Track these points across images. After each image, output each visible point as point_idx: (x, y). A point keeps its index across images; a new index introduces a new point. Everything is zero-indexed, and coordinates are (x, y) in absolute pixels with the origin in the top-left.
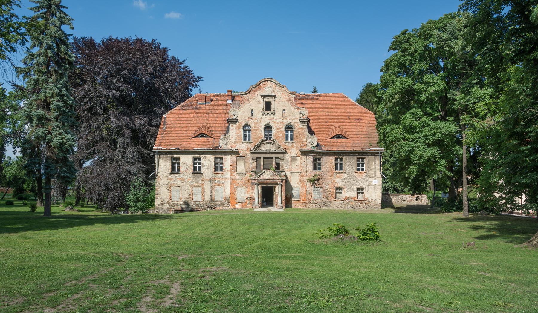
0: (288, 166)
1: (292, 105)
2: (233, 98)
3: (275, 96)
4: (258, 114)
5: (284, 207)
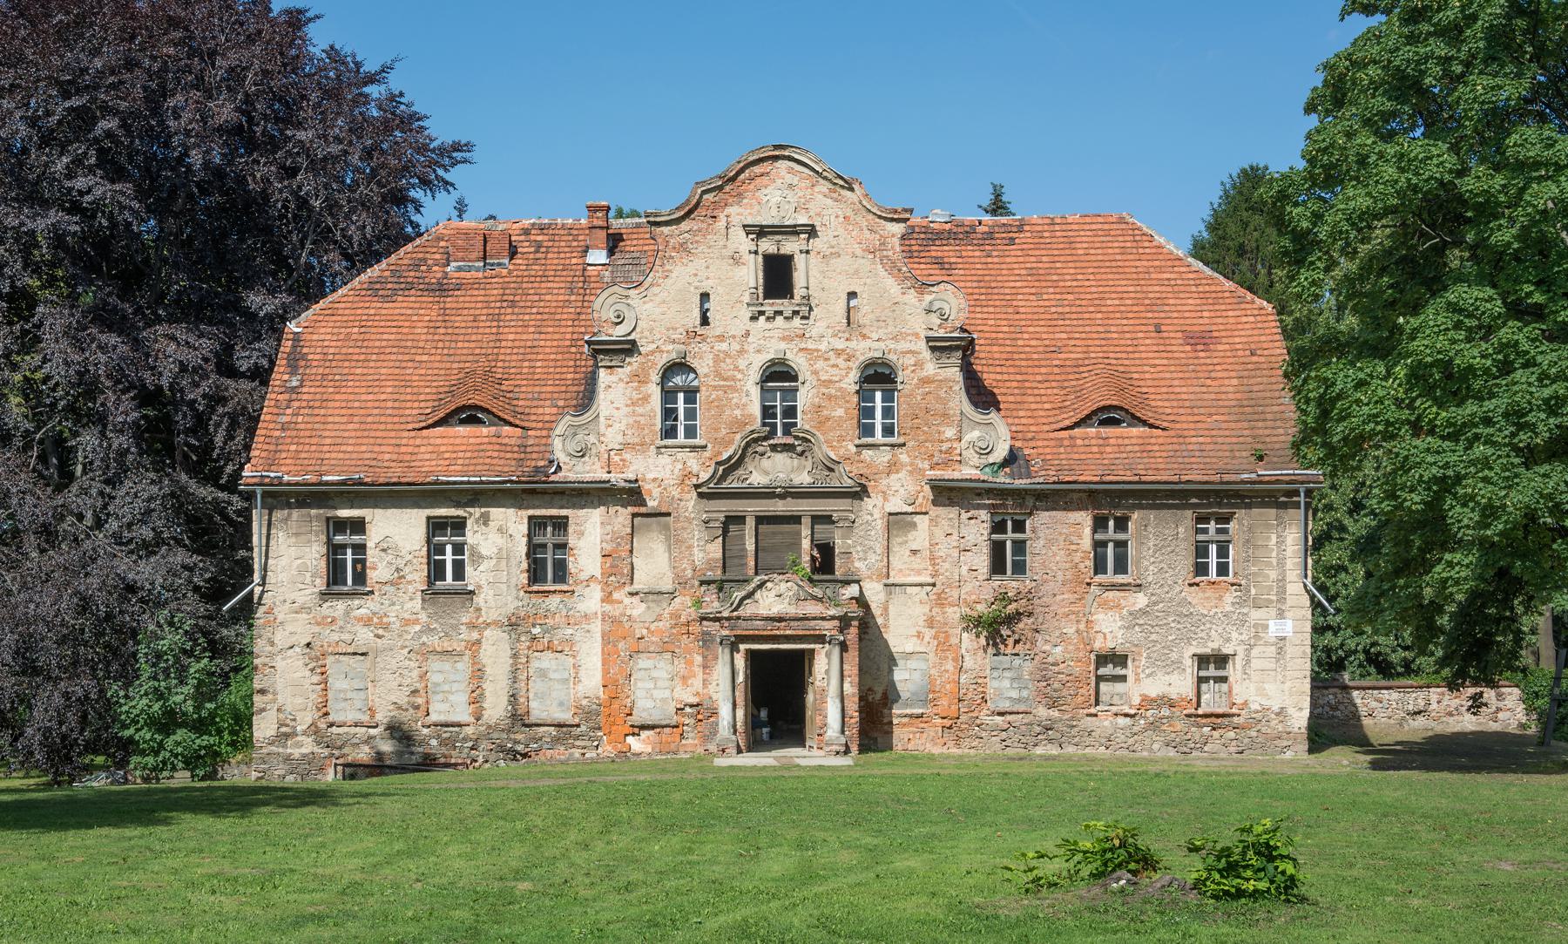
0: (872, 558)
5: (854, 748)
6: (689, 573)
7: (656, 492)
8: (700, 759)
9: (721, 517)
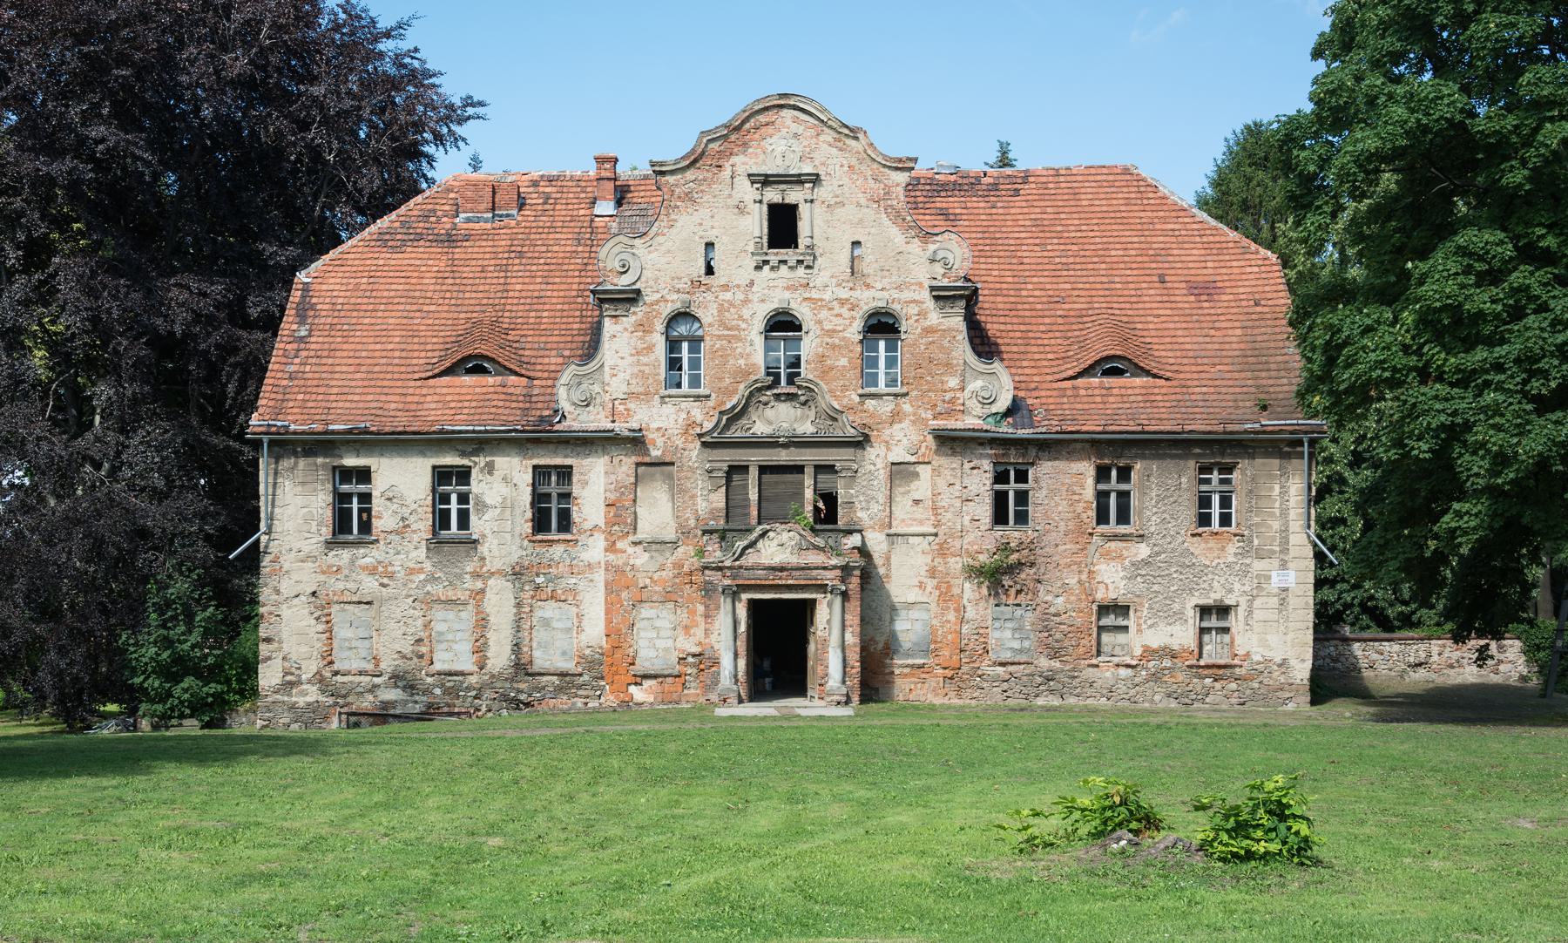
0: (875, 508)
5: (856, 698)
6: (692, 523)
7: (660, 442)
8: (701, 709)
9: (725, 466)
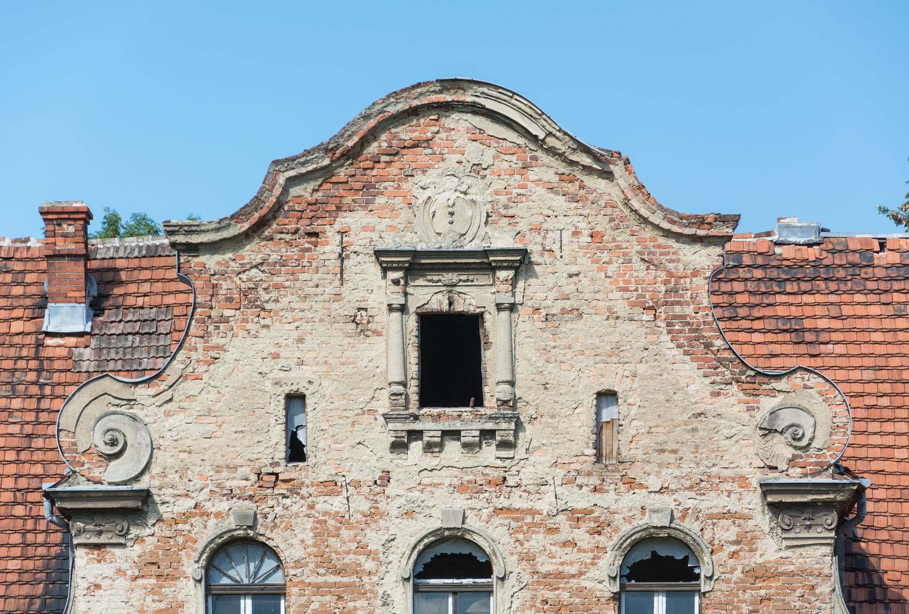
1: (693, 342)
2: (101, 289)
3: (520, 263)
4: (353, 435)
